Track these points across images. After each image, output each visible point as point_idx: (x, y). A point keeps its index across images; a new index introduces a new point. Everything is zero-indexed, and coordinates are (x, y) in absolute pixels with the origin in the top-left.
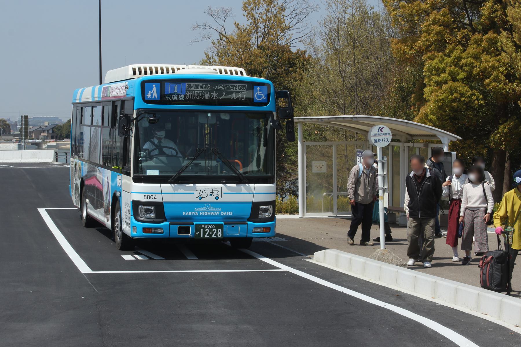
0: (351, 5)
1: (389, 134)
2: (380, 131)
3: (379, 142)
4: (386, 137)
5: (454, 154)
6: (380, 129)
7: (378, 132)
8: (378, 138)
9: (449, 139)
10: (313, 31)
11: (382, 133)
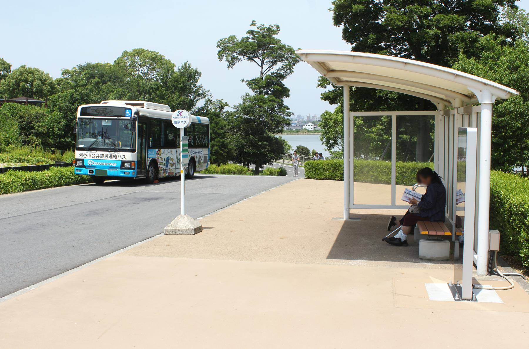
0: (131, 76)
1: (186, 117)
2: (179, 114)
3: (178, 124)
4: (184, 120)
5: (472, 133)
6: (180, 113)
7: (178, 115)
8: (177, 120)
9: (492, 95)
10: (119, 80)
11: (181, 116)
